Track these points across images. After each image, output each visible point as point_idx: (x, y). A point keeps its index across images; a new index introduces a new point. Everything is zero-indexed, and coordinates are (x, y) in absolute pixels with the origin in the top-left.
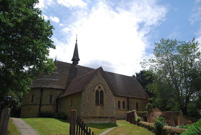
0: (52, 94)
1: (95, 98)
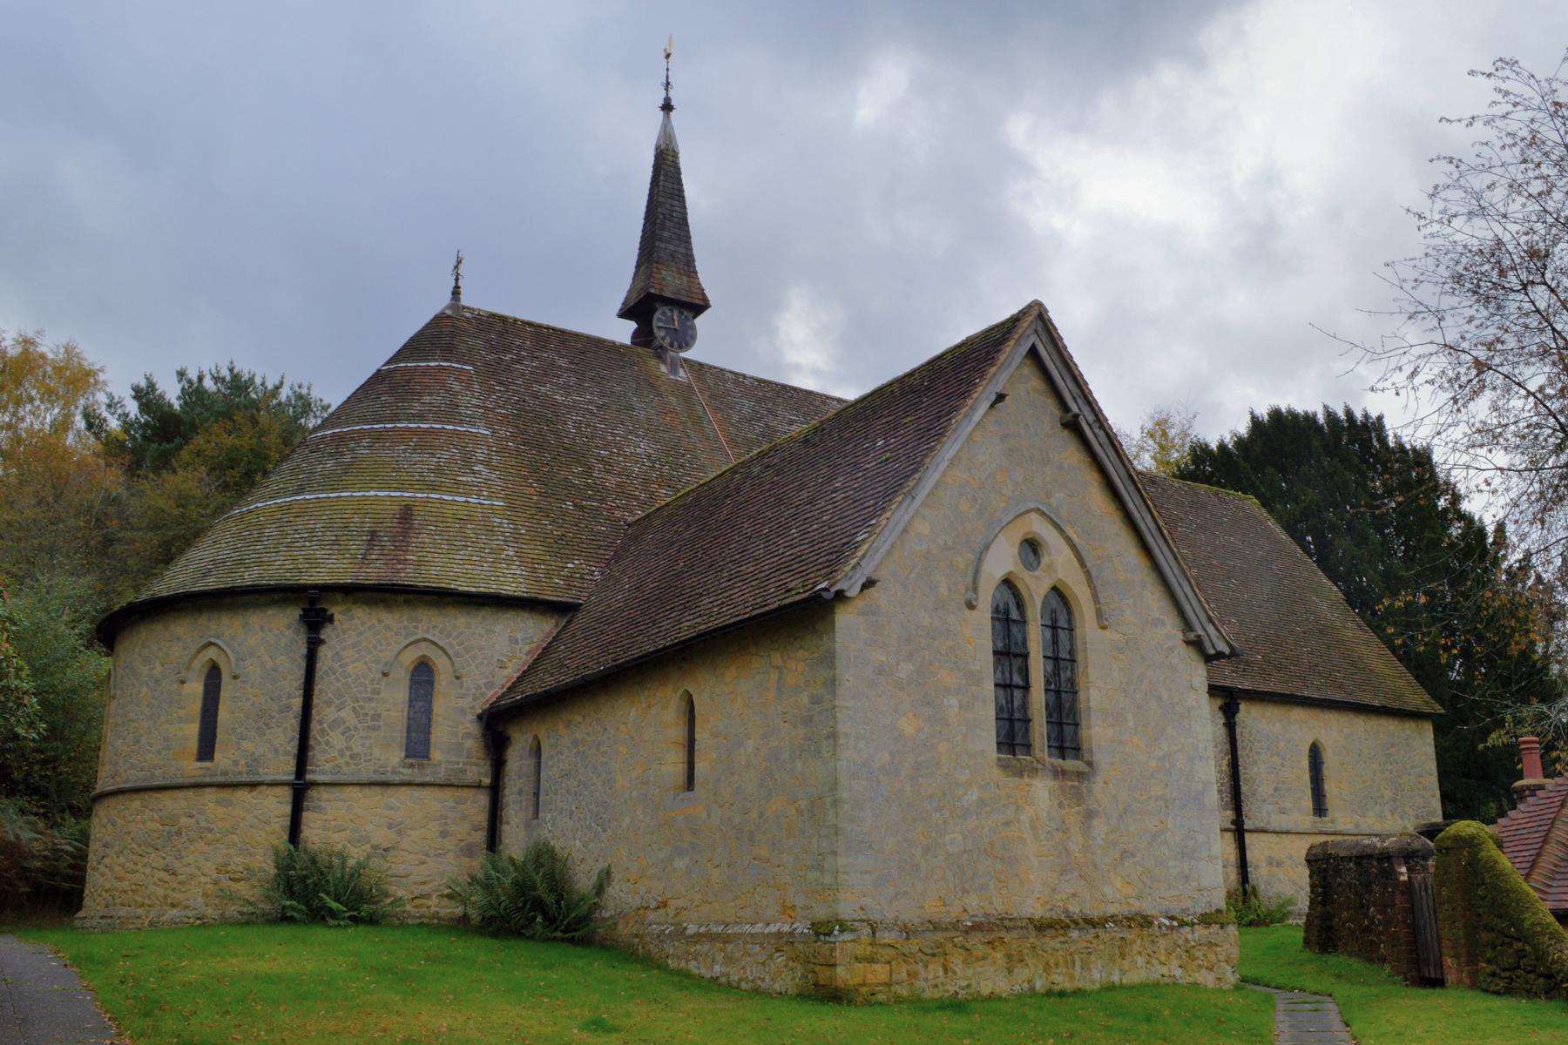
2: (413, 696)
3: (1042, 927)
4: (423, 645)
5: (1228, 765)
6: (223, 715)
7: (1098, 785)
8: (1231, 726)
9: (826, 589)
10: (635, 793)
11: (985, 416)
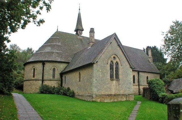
0: (55, 67)
3: (115, 95)
6: (35, 73)
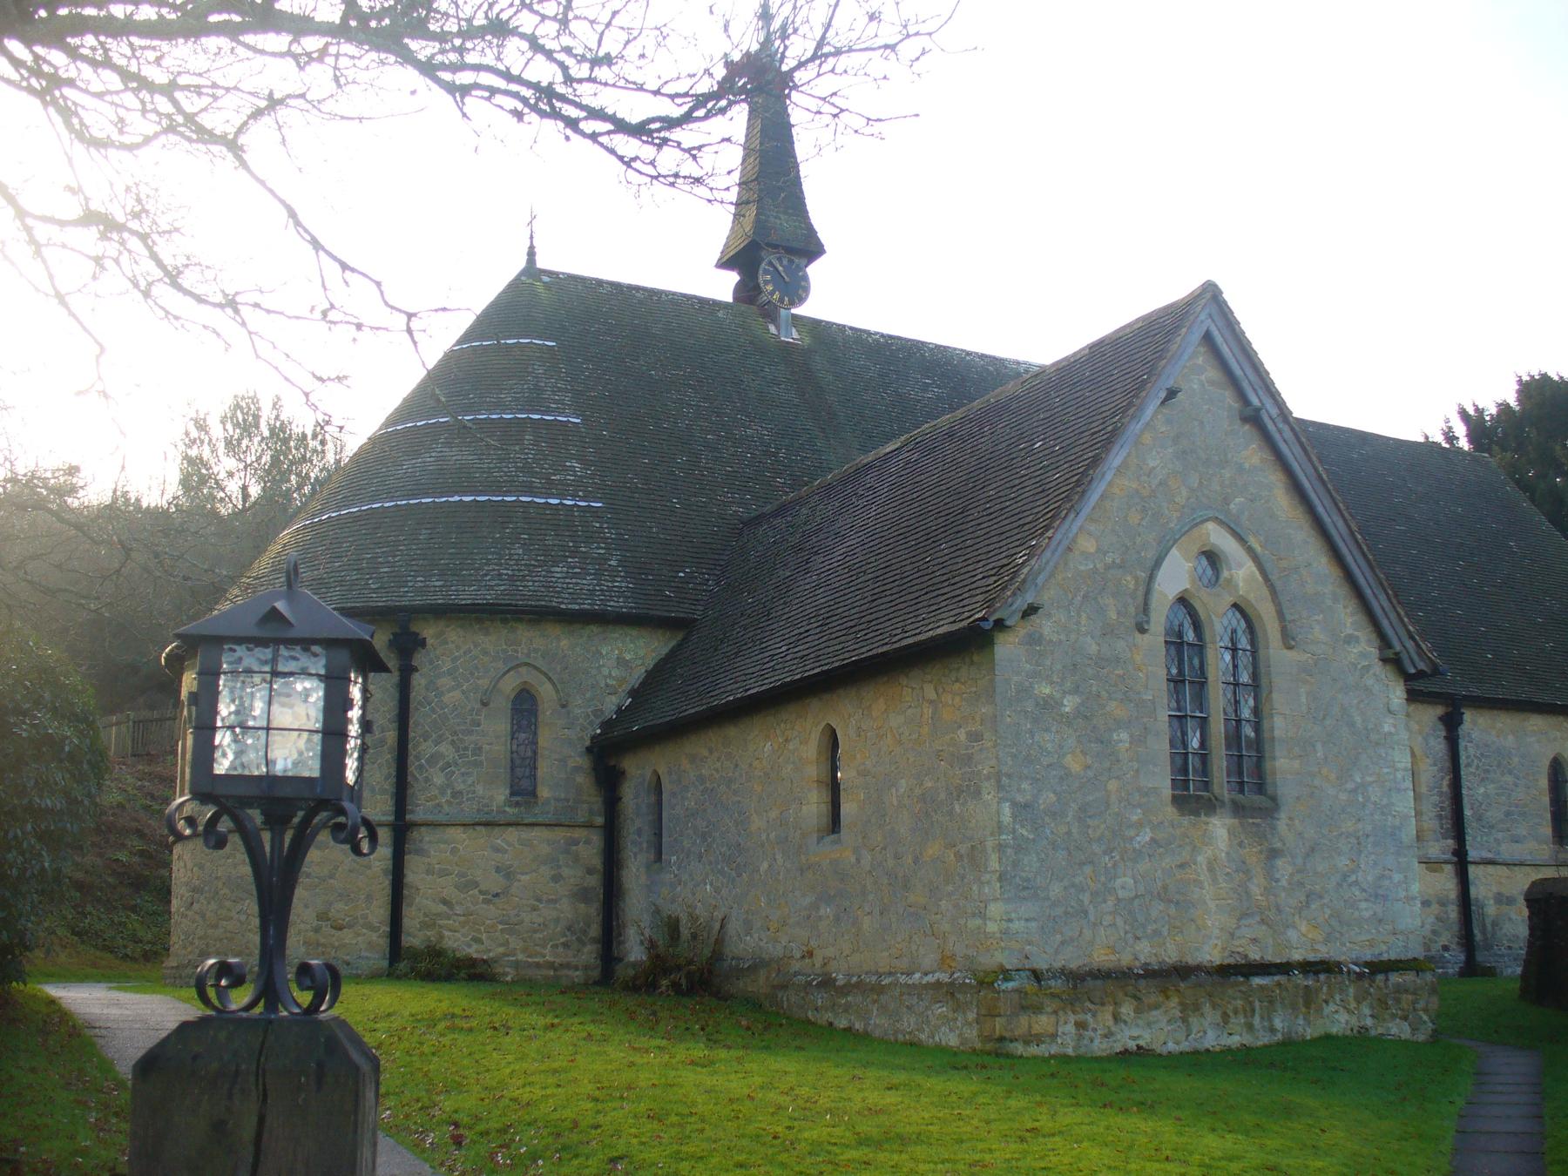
1: (1163, 715)
2: (515, 727)
4: (523, 670)
5: (1449, 786)
7: (1282, 825)
8: (1453, 742)
9: (983, 619)
10: (772, 836)
11: (1156, 413)
